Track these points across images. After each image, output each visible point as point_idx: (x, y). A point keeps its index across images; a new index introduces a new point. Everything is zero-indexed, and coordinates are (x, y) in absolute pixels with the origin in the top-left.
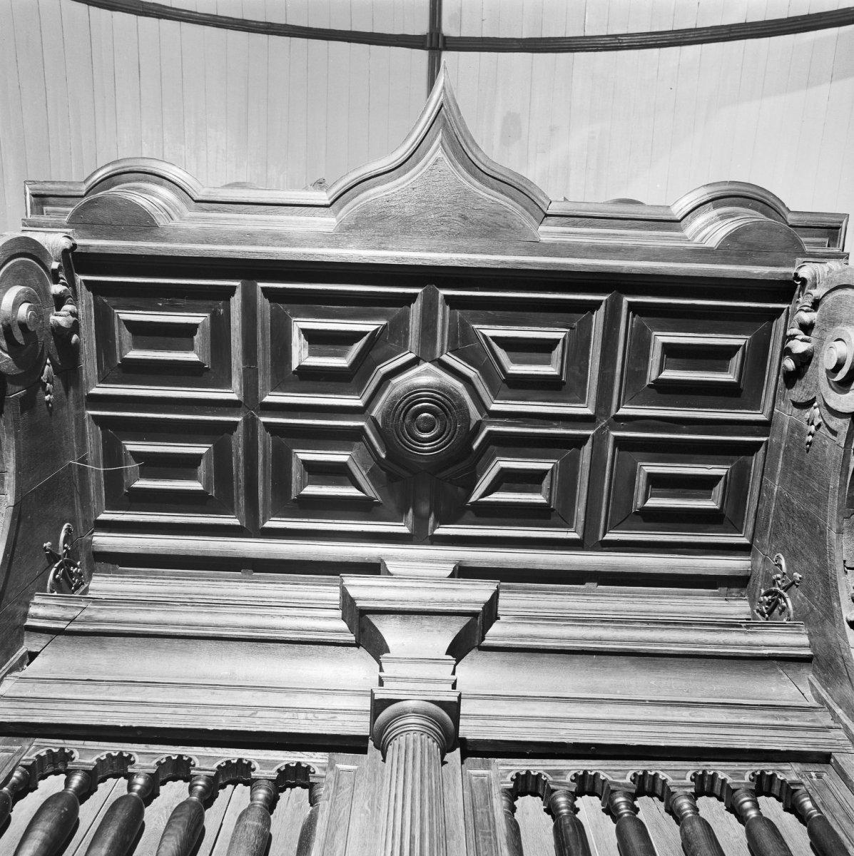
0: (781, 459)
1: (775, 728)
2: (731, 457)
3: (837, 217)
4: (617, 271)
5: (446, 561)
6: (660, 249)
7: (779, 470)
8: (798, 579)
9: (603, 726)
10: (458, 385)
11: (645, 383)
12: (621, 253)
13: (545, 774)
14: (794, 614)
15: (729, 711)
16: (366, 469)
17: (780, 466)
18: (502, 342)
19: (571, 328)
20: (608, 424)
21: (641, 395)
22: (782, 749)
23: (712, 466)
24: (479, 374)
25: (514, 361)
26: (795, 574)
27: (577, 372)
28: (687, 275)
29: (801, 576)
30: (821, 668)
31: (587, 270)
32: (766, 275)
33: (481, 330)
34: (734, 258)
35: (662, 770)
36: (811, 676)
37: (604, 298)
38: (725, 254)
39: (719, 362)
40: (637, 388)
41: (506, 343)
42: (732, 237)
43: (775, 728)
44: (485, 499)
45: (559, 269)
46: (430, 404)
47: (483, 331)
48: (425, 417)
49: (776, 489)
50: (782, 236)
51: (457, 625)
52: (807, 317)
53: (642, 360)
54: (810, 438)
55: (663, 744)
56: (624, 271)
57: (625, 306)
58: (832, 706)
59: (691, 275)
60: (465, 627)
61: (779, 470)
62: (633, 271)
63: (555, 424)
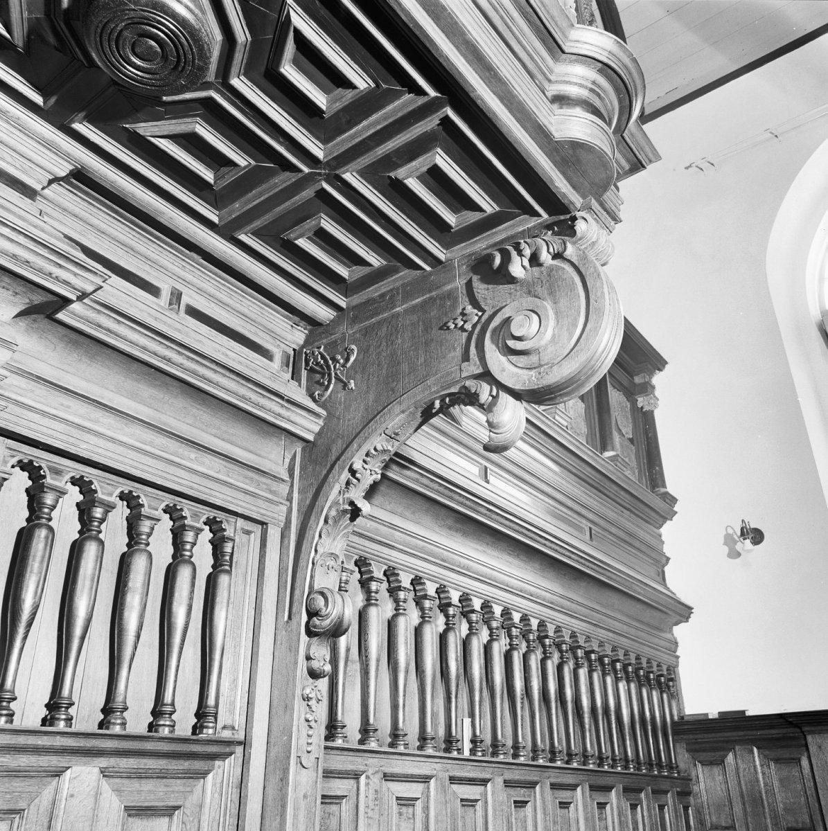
0: (422, 298)
1: (246, 492)
2: (392, 259)
3: (654, 154)
4: (467, 90)
5: (67, 157)
6: (520, 101)
7: (414, 302)
8: (350, 388)
9: (121, 449)
10: (218, 36)
11: (389, 172)
12: (488, 74)
13: (46, 469)
14: (326, 399)
15: (224, 463)
16: (30, 12)
17: (417, 301)
18: (300, 40)
19: (378, 85)
20: (328, 175)
21: (377, 177)
22: (240, 512)
23: (374, 255)
24: (248, 43)
25: (296, 62)
26: (352, 381)
27: (344, 120)
28: (513, 143)
29: (354, 388)
30: (310, 456)
31: (444, 64)
32: (560, 192)
33: (291, 9)
34: (558, 158)
35: (145, 495)
36: (299, 450)
37: (432, 93)
38: (556, 150)
39: (459, 206)
40: (380, 175)
41: (303, 45)
42: (576, 145)
43: (246, 492)
44: (152, 140)
45: (423, 39)
46: (166, 38)
47: (292, 13)
48: (151, 47)
49: (397, 309)
50: (604, 175)
51: (38, 298)
52: (545, 257)
53: (406, 157)
54: (452, 326)
55: (158, 483)
56: (472, 95)
57: (440, 114)
58: (295, 485)
59: (516, 145)
60: (46, 302)
61: (414, 302)
62: (479, 102)
63: (281, 140)
